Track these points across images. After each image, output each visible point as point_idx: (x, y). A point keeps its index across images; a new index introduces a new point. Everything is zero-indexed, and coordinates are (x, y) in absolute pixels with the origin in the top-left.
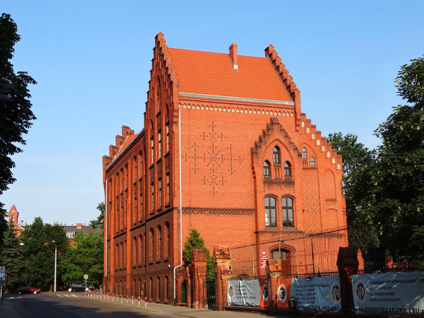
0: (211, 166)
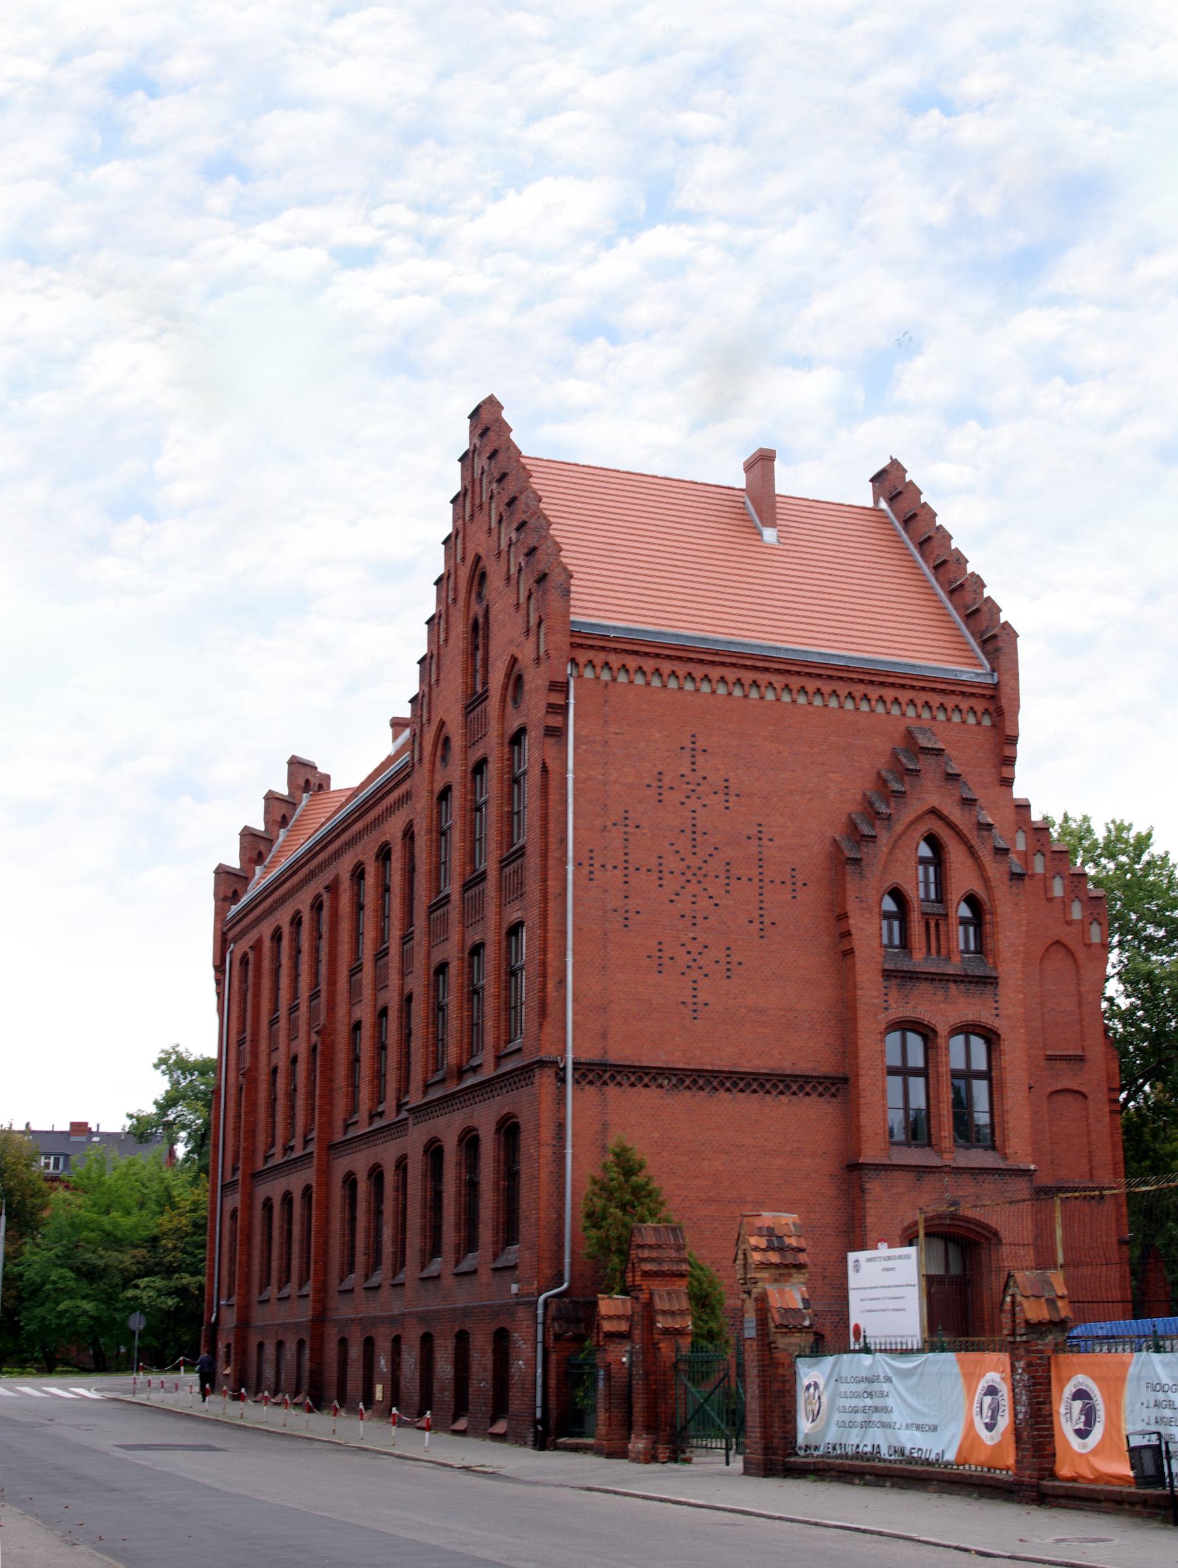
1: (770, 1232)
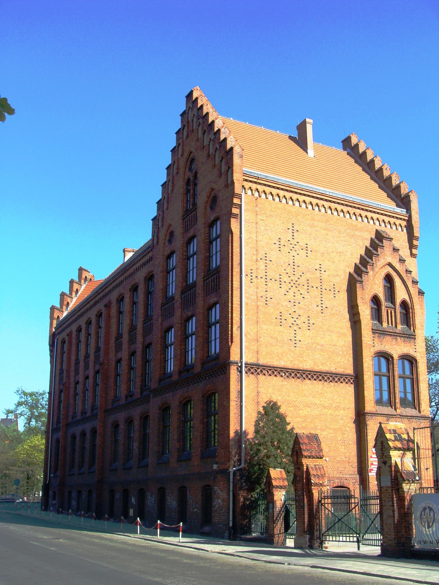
0: (290, 296)
1: (395, 431)
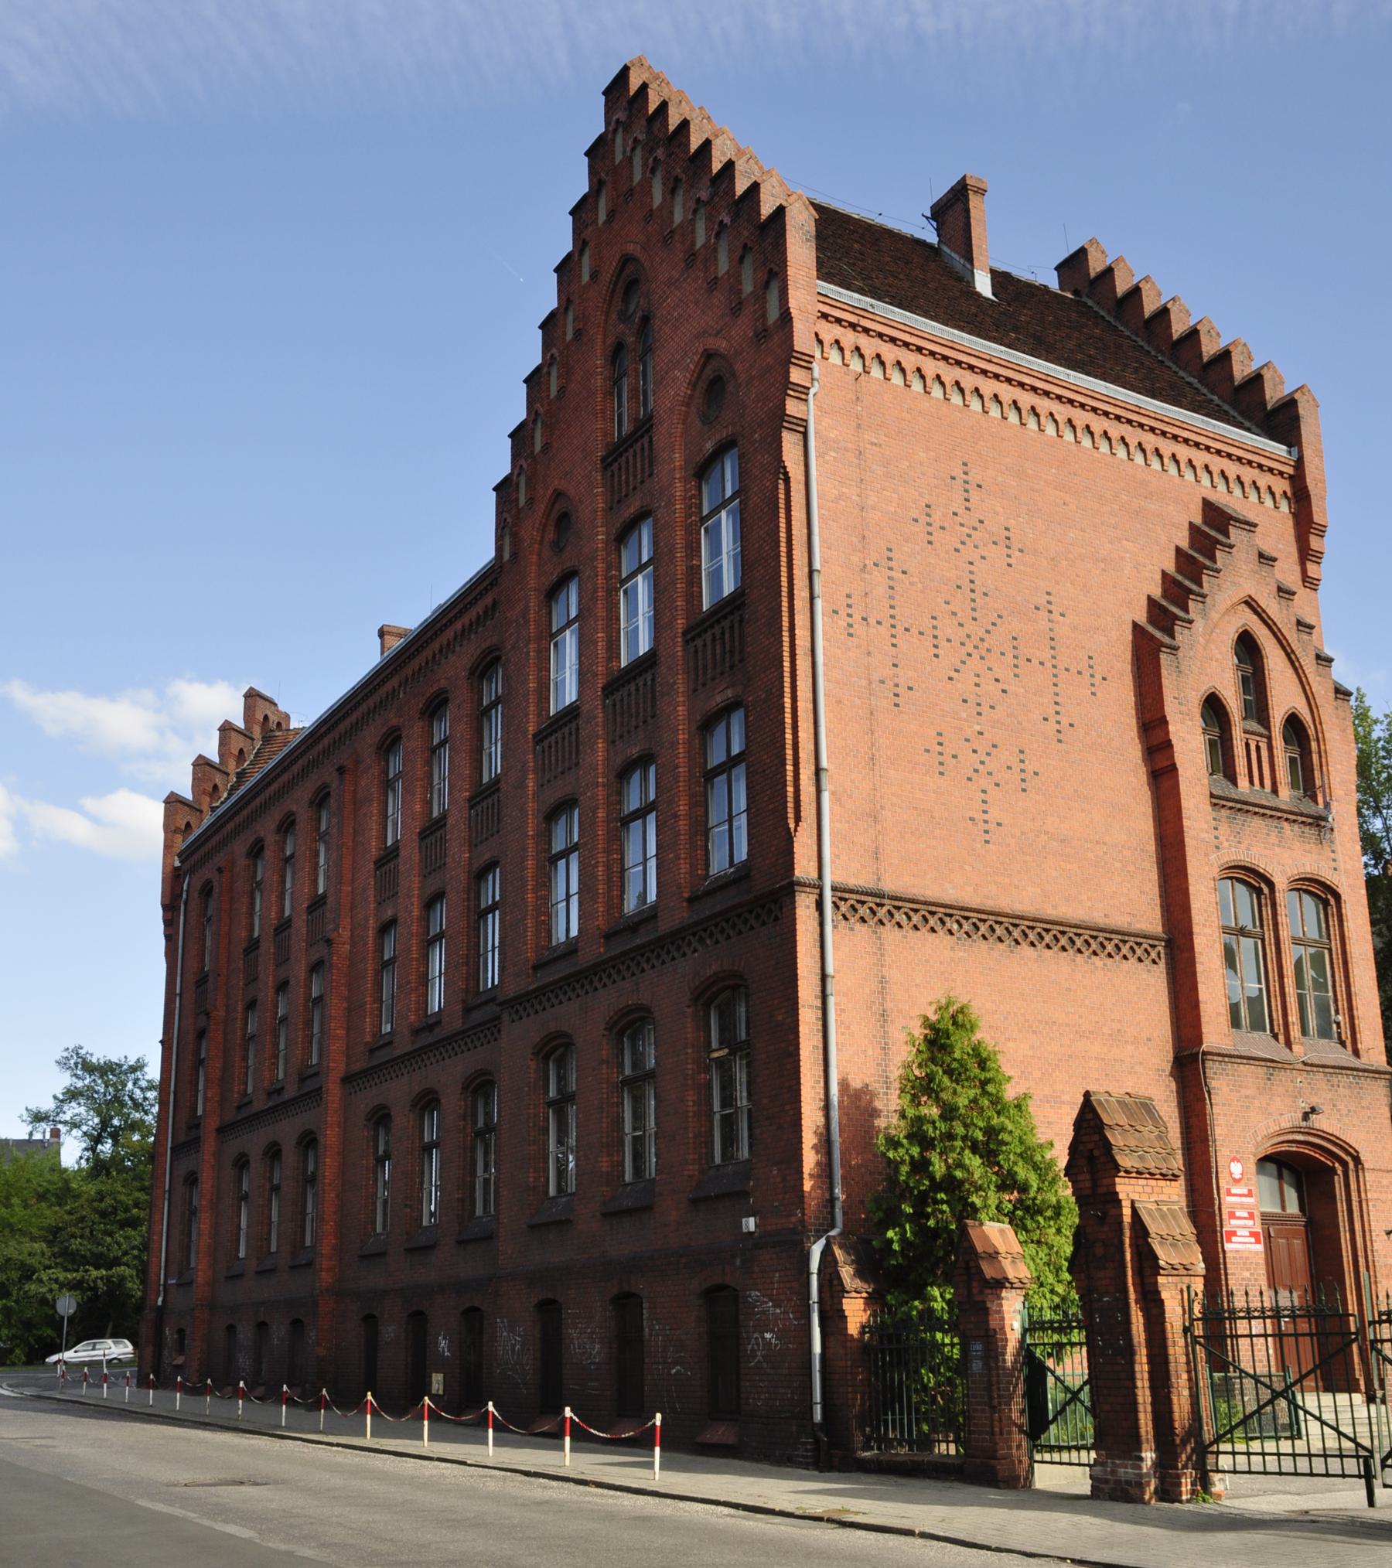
0: (964, 684)
